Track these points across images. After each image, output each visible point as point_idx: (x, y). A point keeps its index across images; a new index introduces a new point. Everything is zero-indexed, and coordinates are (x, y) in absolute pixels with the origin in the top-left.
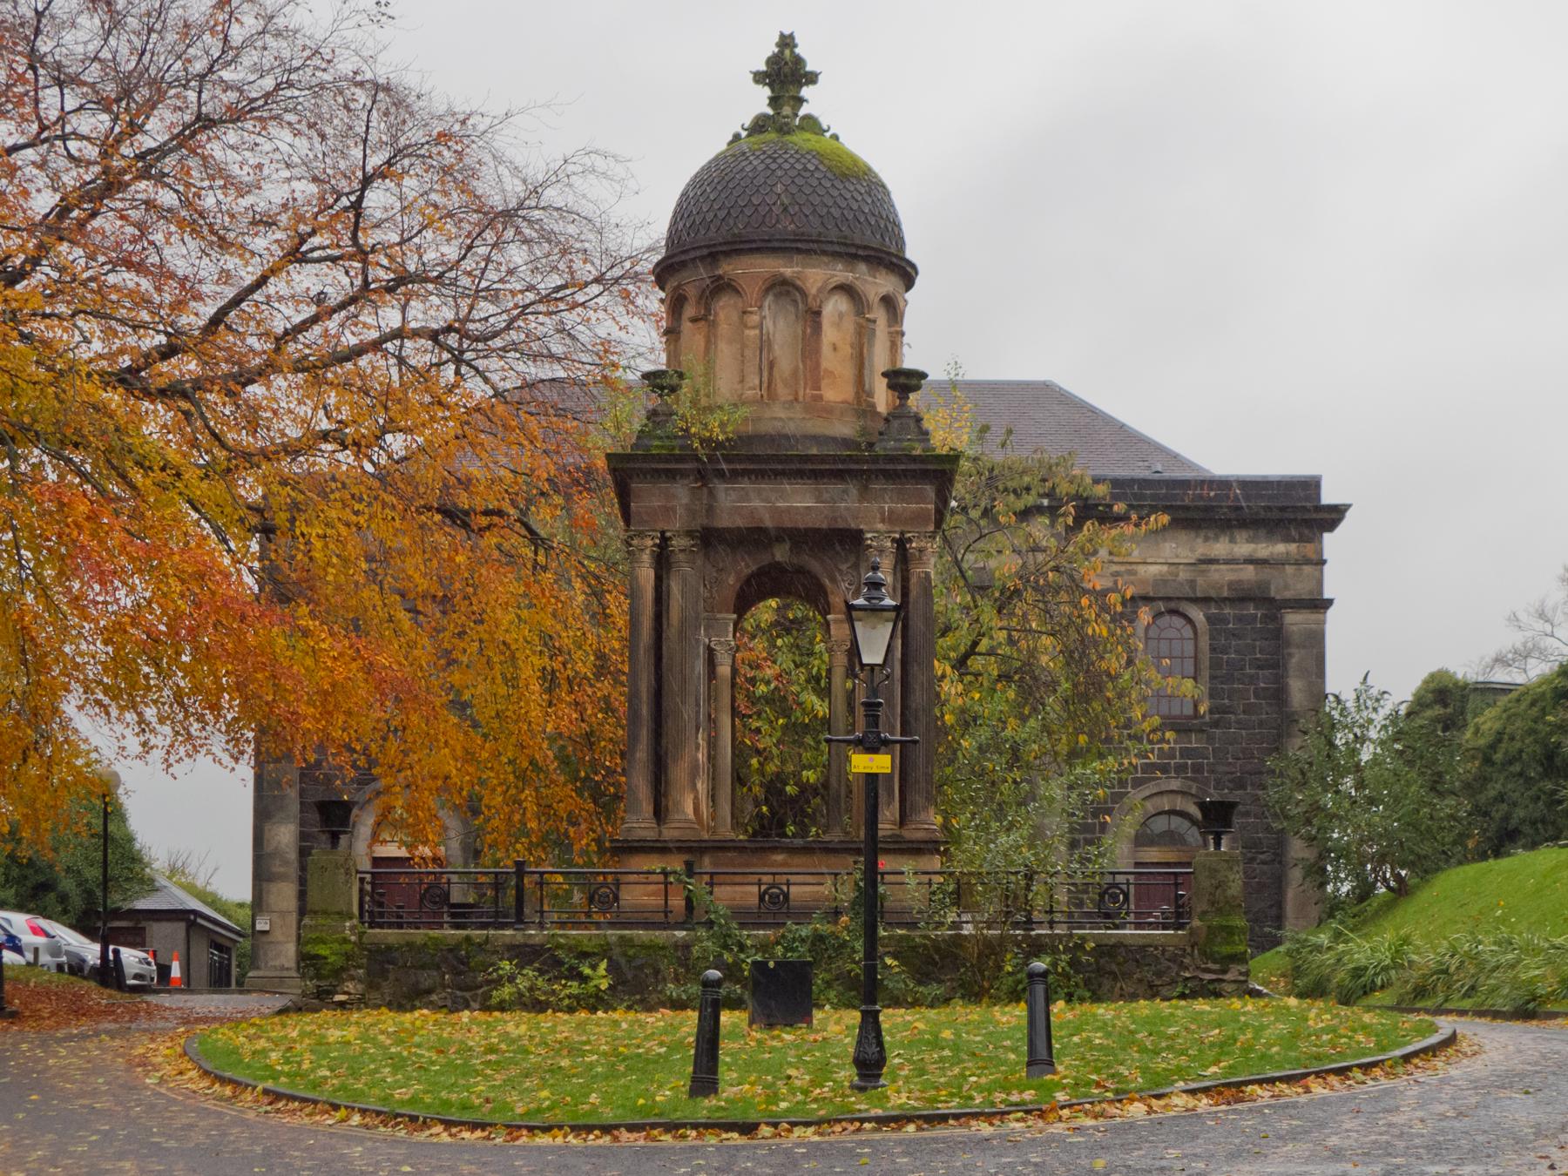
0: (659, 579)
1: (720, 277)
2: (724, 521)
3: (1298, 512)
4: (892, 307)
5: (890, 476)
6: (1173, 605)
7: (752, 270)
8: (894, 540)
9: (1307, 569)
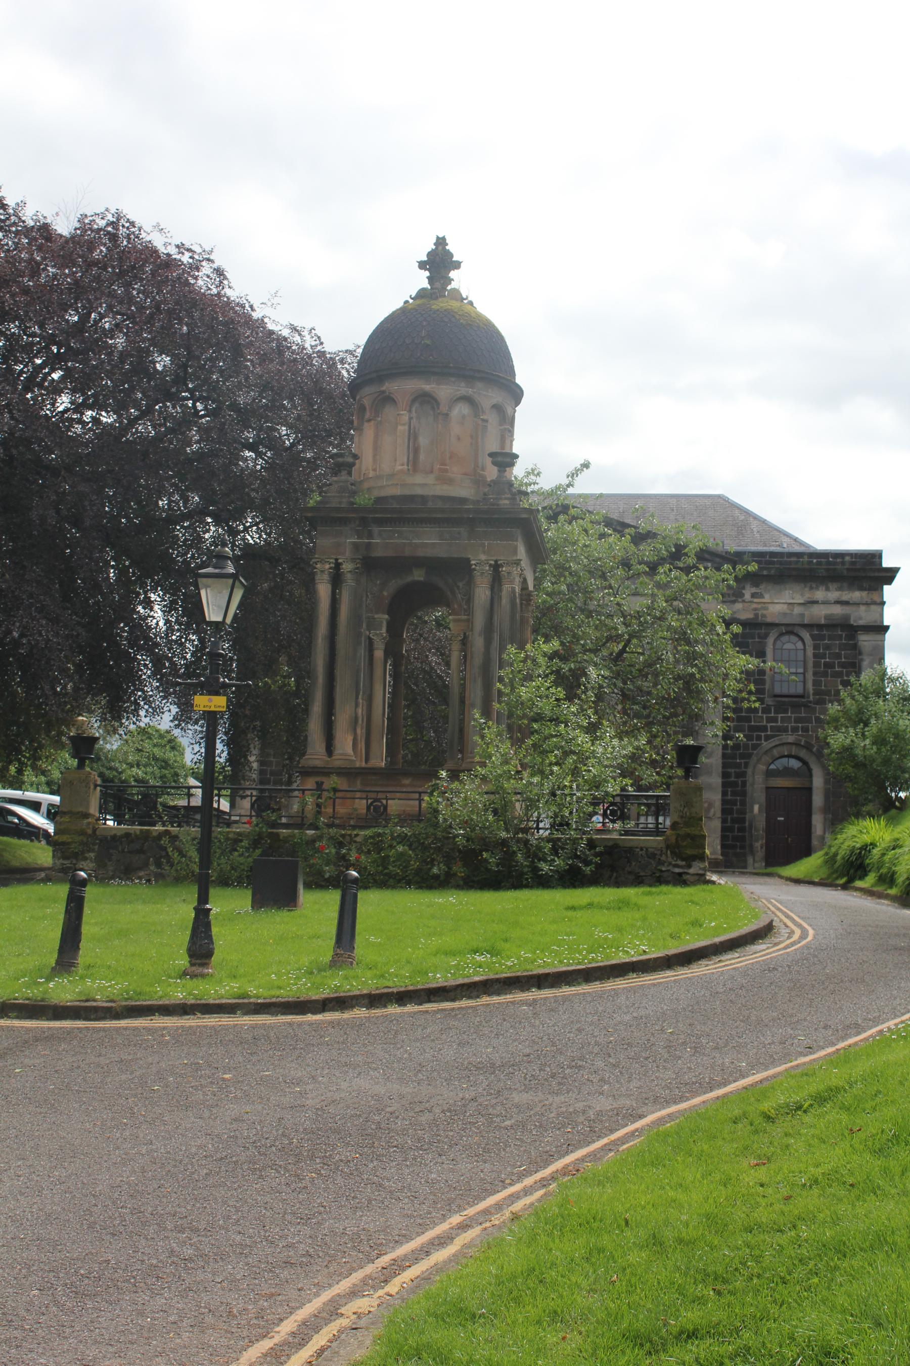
0: (334, 593)
1: (383, 392)
2: (379, 553)
3: (866, 573)
6: (790, 629)
7: (403, 387)
8: (491, 565)
9: (873, 607)
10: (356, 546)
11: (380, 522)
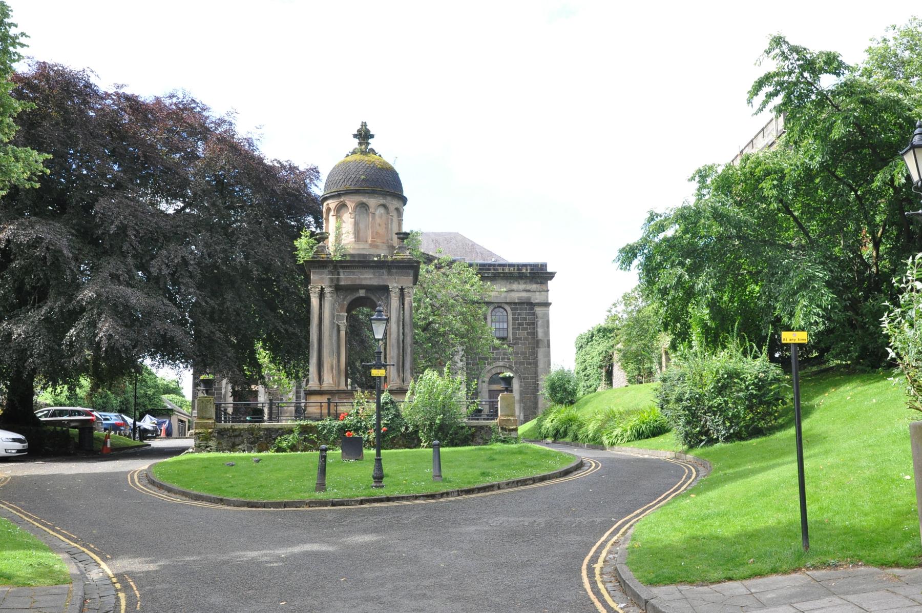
0: (321, 305)
2: (342, 283)
3: (539, 275)
4: (399, 213)
5: (398, 267)
10: (332, 280)
11: (343, 267)
